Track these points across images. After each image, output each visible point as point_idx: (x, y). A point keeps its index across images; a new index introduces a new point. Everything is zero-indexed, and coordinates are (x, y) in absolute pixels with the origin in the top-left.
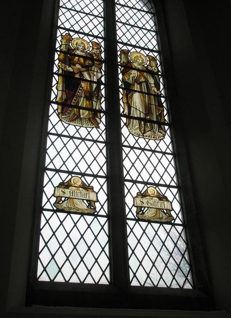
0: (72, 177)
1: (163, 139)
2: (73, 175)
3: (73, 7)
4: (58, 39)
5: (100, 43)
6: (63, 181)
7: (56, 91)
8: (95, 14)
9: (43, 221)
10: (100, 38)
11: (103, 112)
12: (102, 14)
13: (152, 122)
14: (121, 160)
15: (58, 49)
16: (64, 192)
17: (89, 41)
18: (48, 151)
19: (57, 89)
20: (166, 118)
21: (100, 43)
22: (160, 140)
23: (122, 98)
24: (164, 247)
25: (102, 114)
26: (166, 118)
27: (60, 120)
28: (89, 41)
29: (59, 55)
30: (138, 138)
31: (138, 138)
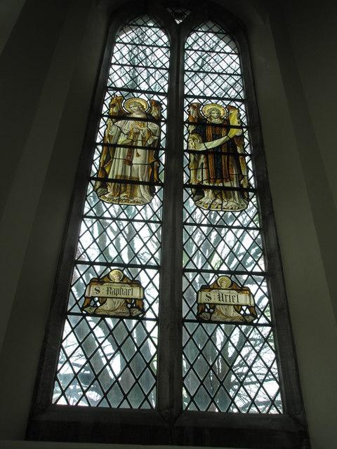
0: (219, 277)
1: (244, 210)
2: (220, 275)
3: (164, 65)
4: (105, 102)
5: (111, 96)
6: (99, 277)
7: (188, 171)
8: (206, 70)
9: (185, 337)
10: (239, 100)
11: (253, 190)
12: (239, 72)
13: (134, 183)
14: (162, 246)
15: (245, 130)
16: (99, 291)
17: (147, 100)
18: (80, 239)
19: (189, 169)
20: (252, 181)
21: (111, 96)
22: (241, 211)
23: (188, 165)
24: (261, 389)
25: (157, 188)
26: (252, 181)
27: (198, 207)
28: (147, 100)
29: (188, 127)
30: (110, 205)
31: (110, 205)
